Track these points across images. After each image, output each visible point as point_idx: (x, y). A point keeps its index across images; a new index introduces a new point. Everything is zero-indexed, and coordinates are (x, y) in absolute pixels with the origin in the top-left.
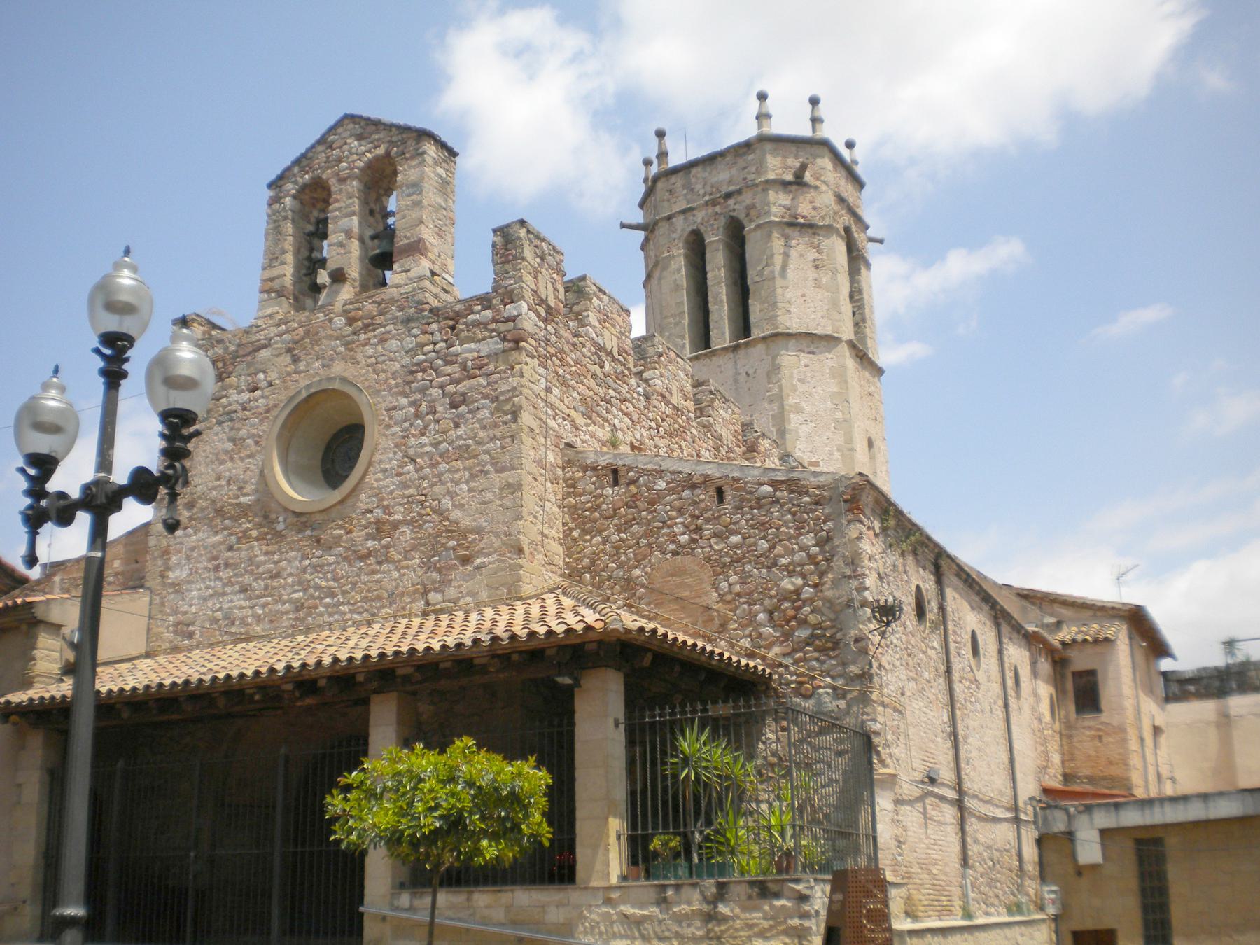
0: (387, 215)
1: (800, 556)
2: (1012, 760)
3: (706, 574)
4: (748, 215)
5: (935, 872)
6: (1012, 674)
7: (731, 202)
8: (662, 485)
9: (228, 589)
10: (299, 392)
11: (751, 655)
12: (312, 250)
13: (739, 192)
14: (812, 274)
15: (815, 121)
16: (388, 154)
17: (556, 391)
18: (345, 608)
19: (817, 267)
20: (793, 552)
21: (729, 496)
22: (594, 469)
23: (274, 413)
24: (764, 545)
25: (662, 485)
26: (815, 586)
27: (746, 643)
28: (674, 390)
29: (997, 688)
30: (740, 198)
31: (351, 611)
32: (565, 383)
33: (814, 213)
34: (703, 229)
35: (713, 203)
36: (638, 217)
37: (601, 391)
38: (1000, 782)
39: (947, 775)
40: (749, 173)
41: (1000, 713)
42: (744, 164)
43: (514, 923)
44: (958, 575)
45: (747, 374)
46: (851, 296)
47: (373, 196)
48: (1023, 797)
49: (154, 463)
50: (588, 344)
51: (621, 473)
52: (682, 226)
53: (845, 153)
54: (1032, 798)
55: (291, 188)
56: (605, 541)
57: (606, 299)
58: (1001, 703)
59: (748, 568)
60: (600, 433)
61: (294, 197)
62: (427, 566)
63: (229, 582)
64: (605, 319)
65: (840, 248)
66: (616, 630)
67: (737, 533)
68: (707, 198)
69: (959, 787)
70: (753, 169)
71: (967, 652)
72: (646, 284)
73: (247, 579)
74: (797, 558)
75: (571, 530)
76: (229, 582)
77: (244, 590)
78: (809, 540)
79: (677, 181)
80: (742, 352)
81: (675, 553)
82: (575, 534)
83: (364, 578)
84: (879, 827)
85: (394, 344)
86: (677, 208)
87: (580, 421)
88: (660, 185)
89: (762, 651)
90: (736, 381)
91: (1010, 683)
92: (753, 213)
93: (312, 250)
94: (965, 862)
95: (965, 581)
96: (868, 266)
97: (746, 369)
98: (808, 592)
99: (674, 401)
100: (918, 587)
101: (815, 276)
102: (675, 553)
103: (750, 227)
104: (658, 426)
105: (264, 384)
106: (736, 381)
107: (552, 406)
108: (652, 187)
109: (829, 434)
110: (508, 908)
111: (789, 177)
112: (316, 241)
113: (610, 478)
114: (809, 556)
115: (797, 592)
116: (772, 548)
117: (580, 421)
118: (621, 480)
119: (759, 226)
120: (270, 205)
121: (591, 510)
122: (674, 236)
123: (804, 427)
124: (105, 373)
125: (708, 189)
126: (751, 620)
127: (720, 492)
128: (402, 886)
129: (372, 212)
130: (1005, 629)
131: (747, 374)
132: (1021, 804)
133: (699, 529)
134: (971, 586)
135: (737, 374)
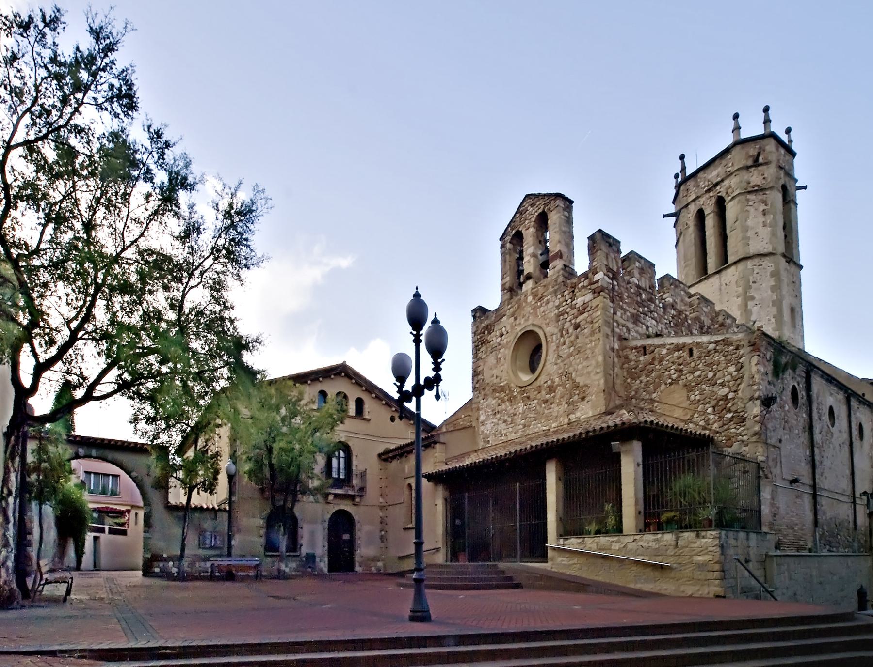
0: (546, 241)
1: (728, 378)
2: (853, 473)
3: (684, 393)
4: (727, 193)
5: (796, 529)
6: (857, 427)
7: (718, 188)
8: (664, 351)
9: (500, 422)
10: (518, 334)
11: (704, 428)
12: (519, 266)
13: (722, 181)
14: (761, 219)
15: (767, 121)
16: (543, 211)
17: (619, 314)
18: (539, 425)
19: (764, 214)
20: (724, 376)
21: (696, 353)
22: (636, 348)
23: (509, 344)
24: (711, 375)
25: (664, 351)
26: (735, 392)
27: (702, 423)
28: (678, 301)
29: (845, 436)
30: (723, 184)
31: (542, 426)
32: (622, 308)
33: (764, 181)
34: (703, 207)
35: (709, 191)
36: (672, 209)
37: (641, 310)
38: (844, 484)
39: (806, 479)
40: (728, 167)
41: (846, 449)
42: (725, 163)
43: (600, 550)
44: (822, 377)
45: (726, 285)
46: (784, 228)
47: (540, 234)
48: (859, 491)
49: (432, 374)
50: (634, 287)
51: (647, 348)
52: (693, 209)
53: (784, 138)
54: (865, 493)
55: (508, 238)
56: (641, 382)
57: (642, 261)
58: (848, 443)
59: (704, 386)
60: (639, 329)
61: (510, 242)
62: (568, 403)
63: (499, 420)
64: (642, 271)
65: (779, 197)
66: (635, 423)
67: (698, 370)
68: (706, 189)
69: (814, 486)
70: (730, 164)
71: (826, 417)
72: (676, 245)
73: (506, 417)
74: (726, 379)
75: (627, 379)
76: (499, 420)
77: (505, 421)
78: (732, 369)
79: (691, 183)
80: (724, 273)
81: (671, 384)
82: (629, 380)
83: (546, 411)
84: (763, 507)
85: (551, 305)
86: (691, 199)
87: (631, 325)
88: (682, 188)
89: (709, 427)
90: (720, 289)
91: (855, 432)
92: (730, 191)
93: (519, 266)
94: (816, 523)
95: (827, 380)
96: (796, 204)
97: (725, 282)
98: (731, 395)
99: (678, 307)
100: (794, 387)
101: (764, 220)
102: (671, 384)
103: (727, 199)
104: (670, 322)
105: (505, 333)
106: (720, 289)
107: (617, 322)
108: (678, 187)
109: (768, 309)
110: (597, 543)
111: (750, 162)
112: (521, 262)
113: (642, 352)
114: (732, 377)
115: (727, 396)
116: (715, 375)
117: (631, 325)
118: (647, 352)
119: (733, 198)
120: (501, 248)
121: (635, 368)
122: (689, 215)
123: (755, 308)
124: (414, 341)
125: (706, 184)
126: (704, 412)
127: (691, 351)
128: (561, 536)
129: (540, 242)
130: (854, 403)
131: (726, 285)
132: (857, 495)
133: (681, 371)
134: (831, 382)
135: (721, 285)
